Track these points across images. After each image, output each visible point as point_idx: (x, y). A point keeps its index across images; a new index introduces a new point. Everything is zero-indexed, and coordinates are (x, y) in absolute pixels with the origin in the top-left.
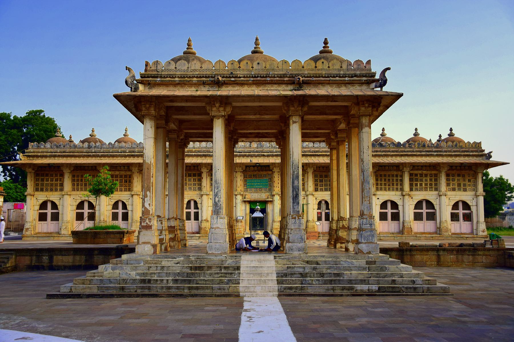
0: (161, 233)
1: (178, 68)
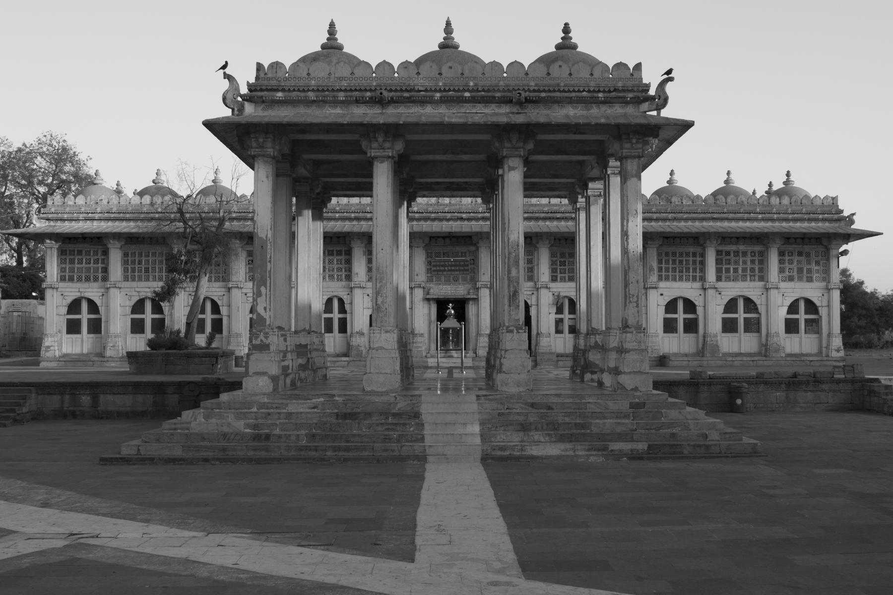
0: (285, 356)
1: (313, 75)
